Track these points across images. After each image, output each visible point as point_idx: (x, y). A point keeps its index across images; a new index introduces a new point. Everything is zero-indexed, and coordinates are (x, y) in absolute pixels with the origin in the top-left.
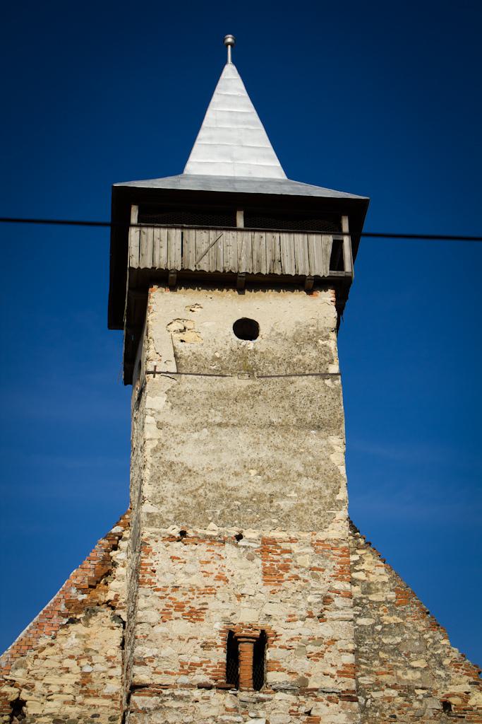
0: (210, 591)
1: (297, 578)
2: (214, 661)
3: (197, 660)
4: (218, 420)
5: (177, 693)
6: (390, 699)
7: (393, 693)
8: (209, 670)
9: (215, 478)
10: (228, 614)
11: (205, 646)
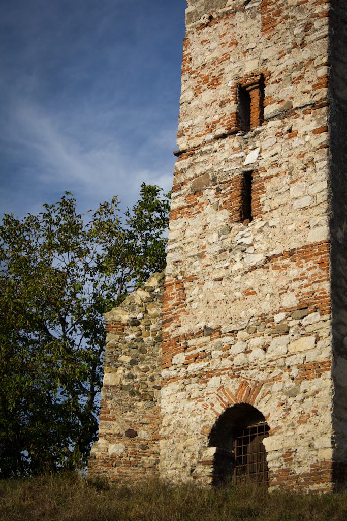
0: (226, 57)
1: (287, 17)
2: (228, 114)
3: (217, 117)
5: (203, 149)
8: (225, 123)
10: (236, 71)
11: (222, 104)
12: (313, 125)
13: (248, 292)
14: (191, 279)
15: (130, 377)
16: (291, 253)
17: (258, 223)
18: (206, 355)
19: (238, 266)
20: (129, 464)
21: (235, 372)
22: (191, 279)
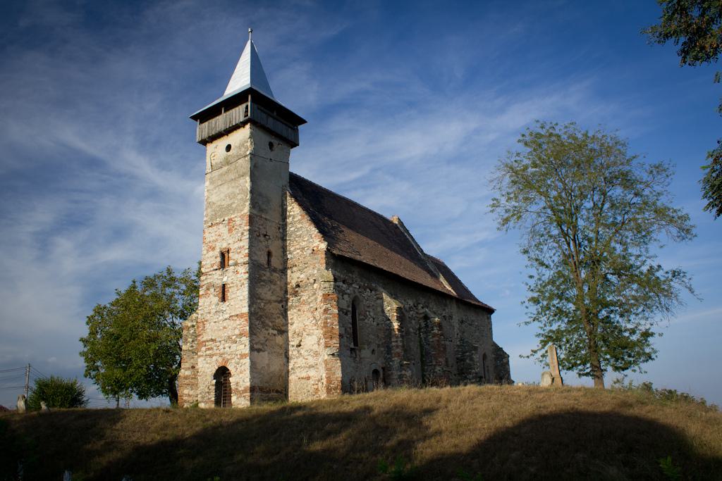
4: (220, 183)
6: (298, 253)
7: (299, 251)
9: (219, 203)
11: (216, 258)
12: (244, 271)
13: (225, 328)
14: (206, 321)
15: (192, 346)
16: (237, 315)
17: (227, 303)
18: (211, 349)
19: (221, 318)
20: (192, 378)
21: (221, 355)
22: (206, 321)
